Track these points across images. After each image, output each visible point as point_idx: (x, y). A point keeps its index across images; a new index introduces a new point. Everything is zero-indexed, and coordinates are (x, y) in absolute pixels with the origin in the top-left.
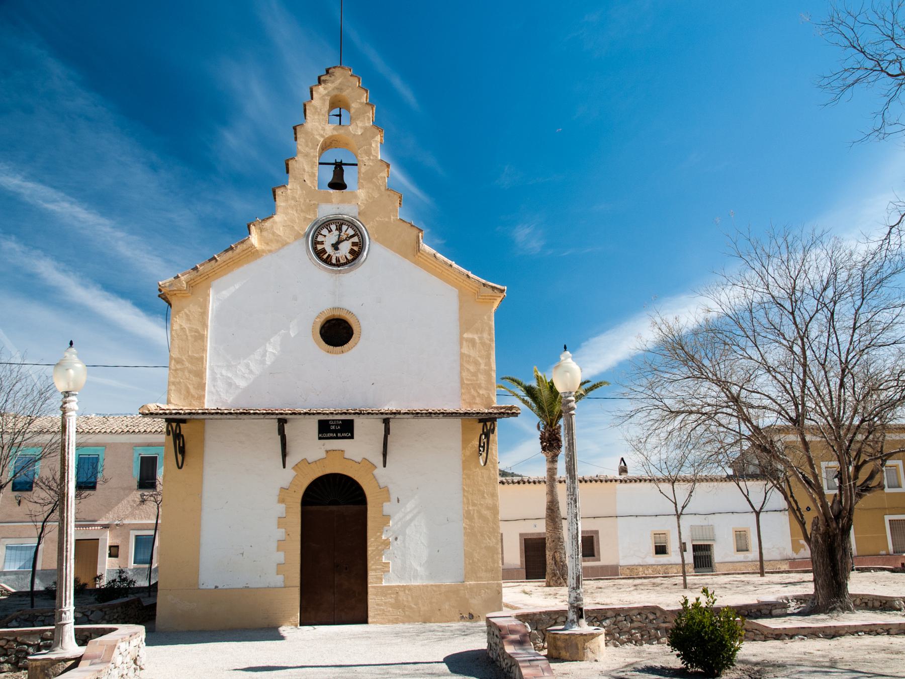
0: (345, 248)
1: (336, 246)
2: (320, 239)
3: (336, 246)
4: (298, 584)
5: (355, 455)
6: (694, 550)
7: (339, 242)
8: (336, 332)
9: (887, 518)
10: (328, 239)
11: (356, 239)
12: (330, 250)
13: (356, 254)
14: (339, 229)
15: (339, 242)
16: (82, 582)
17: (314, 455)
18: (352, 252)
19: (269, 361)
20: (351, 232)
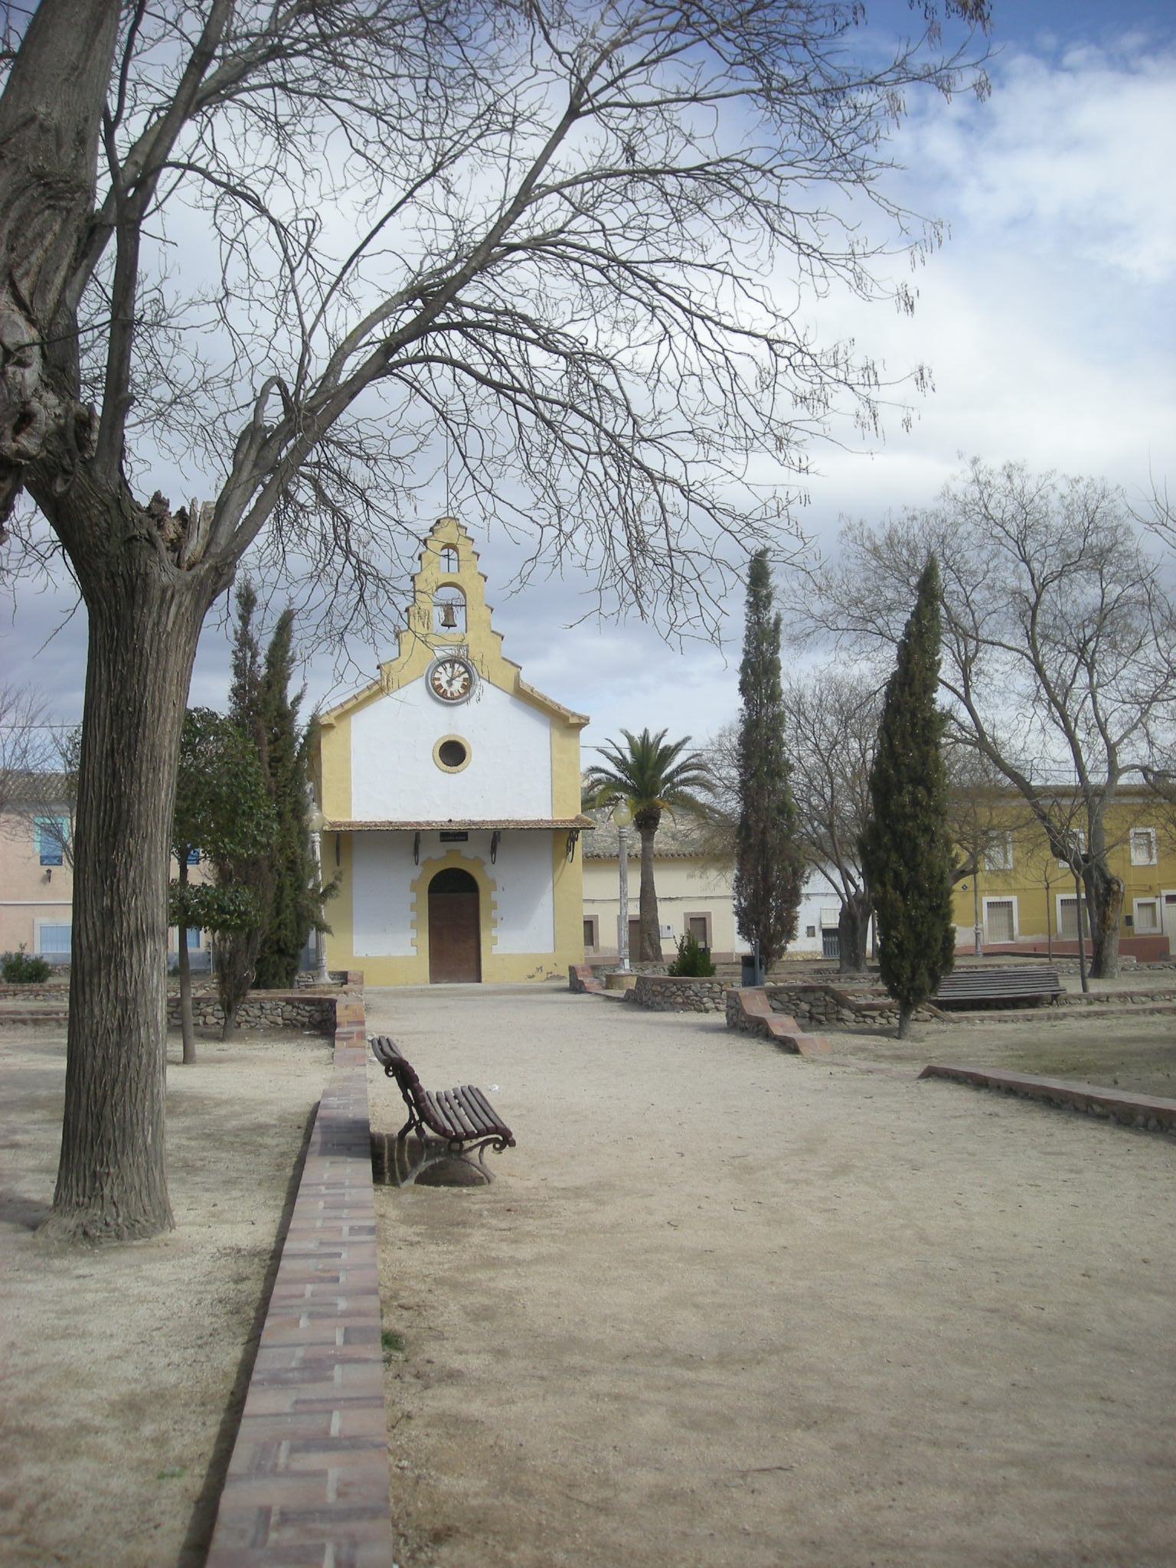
0: (457, 685)
1: (450, 683)
2: (437, 675)
3: (450, 683)
4: (108, 189)
5: (465, 857)
6: (824, 935)
7: (452, 679)
8: (453, 753)
9: (1013, 899)
10: (443, 677)
11: (466, 675)
12: (445, 686)
13: (468, 686)
14: (453, 667)
15: (452, 679)
16: (637, 734)
17: (439, 858)
18: (463, 686)
19: (401, 326)
20: (462, 669)
